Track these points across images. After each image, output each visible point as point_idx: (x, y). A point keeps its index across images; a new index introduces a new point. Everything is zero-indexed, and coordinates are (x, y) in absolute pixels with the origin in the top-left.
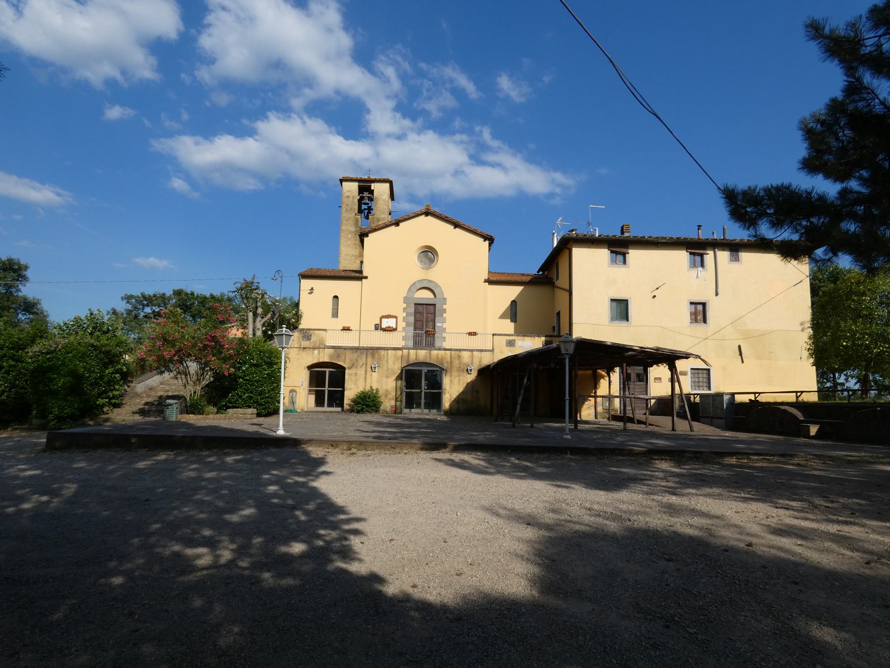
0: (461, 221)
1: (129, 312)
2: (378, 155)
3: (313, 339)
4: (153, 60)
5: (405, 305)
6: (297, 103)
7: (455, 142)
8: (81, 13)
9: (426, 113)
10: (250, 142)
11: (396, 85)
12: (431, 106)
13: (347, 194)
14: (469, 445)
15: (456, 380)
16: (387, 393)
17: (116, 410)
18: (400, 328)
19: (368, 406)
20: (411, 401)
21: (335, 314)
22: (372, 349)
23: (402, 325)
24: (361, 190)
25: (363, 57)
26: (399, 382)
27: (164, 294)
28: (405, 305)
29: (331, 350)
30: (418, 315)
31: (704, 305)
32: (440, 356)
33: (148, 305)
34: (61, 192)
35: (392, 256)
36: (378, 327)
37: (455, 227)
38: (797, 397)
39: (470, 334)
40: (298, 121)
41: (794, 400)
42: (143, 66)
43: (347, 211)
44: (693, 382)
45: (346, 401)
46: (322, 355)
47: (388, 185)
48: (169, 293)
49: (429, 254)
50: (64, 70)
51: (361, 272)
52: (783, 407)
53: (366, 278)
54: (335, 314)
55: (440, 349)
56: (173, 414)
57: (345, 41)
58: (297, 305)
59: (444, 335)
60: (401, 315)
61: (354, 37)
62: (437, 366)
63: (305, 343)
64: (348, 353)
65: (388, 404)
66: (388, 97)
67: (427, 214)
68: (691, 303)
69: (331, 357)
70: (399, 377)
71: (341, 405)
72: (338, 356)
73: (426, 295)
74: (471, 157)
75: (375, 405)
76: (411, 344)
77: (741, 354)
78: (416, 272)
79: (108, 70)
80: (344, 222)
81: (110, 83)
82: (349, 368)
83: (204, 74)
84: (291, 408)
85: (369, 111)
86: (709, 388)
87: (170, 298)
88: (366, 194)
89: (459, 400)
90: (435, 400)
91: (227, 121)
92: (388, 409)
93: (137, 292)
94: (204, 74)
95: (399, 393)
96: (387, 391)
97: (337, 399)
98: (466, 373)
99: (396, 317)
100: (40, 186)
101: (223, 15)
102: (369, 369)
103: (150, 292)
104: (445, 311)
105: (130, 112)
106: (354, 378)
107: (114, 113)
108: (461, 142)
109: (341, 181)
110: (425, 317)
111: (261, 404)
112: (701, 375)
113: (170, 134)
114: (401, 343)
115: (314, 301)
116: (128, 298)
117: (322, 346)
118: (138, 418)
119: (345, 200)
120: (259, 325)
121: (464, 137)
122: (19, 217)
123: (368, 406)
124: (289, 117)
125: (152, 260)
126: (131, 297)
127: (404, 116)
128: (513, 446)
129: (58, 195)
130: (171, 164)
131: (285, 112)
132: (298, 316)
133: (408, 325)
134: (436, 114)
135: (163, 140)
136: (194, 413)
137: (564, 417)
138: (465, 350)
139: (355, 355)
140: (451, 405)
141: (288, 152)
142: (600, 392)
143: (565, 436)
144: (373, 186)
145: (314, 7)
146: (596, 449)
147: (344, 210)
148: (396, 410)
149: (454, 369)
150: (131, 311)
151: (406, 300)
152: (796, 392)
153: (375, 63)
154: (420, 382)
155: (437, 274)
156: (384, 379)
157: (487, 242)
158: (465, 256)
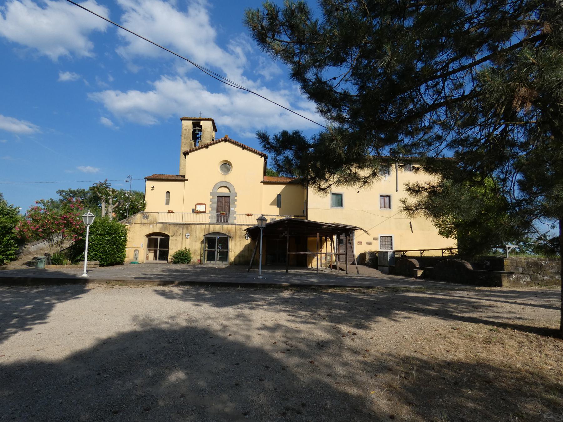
0: (247, 145)
1: (62, 201)
2: (232, 103)
3: (150, 218)
4: (91, 45)
5: (211, 197)
6: (181, 70)
7: (280, 95)
8: (44, 14)
9: (262, 77)
10: (151, 94)
11: (243, 60)
12: (266, 73)
13: (185, 128)
14: (187, 282)
15: (238, 243)
16: (195, 252)
17: (13, 263)
18: (207, 212)
19: (182, 259)
20: (211, 257)
21: (168, 203)
22: (186, 224)
23: (209, 209)
24: (194, 125)
25: (222, 42)
26: (203, 245)
27: (84, 190)
28: (211, 197)
29: (161, 225)
30: (219, 203)
31: (389, 197)
32: (229, 229)
33: (73, 197)
34: (32, 125)
35: (203, 167)
36: (195, 211)
37: (243, 149)
38: (421, 253)
39: (248, 215)
40: (182, 81)
41: (420, 255)
42: (82, 46)
43: (185, 138)
44: (382, 244)
45: (170, 257)
46: (155, 228)
47: (211, 122)
48: (87, 189)
49: (226, 166)
50: (35, 50)
51: (184, 176)
52: (409, 260)
53: (187, 180)
54: (168, 203)
55: (232, 224)
56: (42, 265)
57: (211, 32)
58: (144, 197)
59: (235, 215)
60: (209, 203)
61: (217, 30)
62: (225, 234)
63: (145, 221)
64: (171, 227)
65: (195, 258)
66: (238, 67)
67: (226, 140)
68: (381, 196)
69: (161, 229)
70: (202, 242)
71: (167, 259)
72: (165, 229)
73: (224, 191)
74: (292, 105)
75: (186, 259)
76: (214, 221)
77: (411, 227)
78: (218, 176)
79: (61, 51)
80: (183, 145)
81: (62, 58)
82: (172, 236)
83: (121, 51)
84: (135, 261)
85: (225, 75)
86: (392, 248)
87: (88, 192)
88: (197, 128)
89: (240, 256)
90: (224, 256)
91: (137, 82)
92: (196, 261)
93: (66, 189)
94: (121, 51)
95: (202, 251)
96: (195, 250)
97: (164, 255)
98: (244, 239)
99: (205, 205)
100: (18, 121)
101: (134, 14)
102: (184, 237)
103: (75, 188)
104: (236, 201)
105: (76, 76)
106: (175, 242)
107: (65, 77)
108: (285, 95)
109: (182, 120)
110: (223, 205)
111: (102, 259)
112: (386, 240)
113: (100, 90)
114: (208, 221)
115: (155, 195)
116: (61, 192)
117: (156, 223)
118: (25, 267)
119: (184, 132)
120: (110, 209)
121: (287, 92)
122: (4, 141)
123: (182, 259)
124: (176, 79)
125: (89, 168)
126: (62, 191)
127: (249, 78)
128: (213, 283)
129: (30, 127)
130: (101, 108)
131: (173, 75)
132: (144, 205)
133: (213, 209)
134: (268, 78)
135: (94, 93)
136: (54, 264)
137: (258, 265)
138: (244, 225)
139: (176, 228)
140: (235, 259)
141: (176, 101)
142: (324, 251)
143: (259, 277)
144: (202, 123)
145: (191, 11)
146: (260, 284)
147: (183, 138)
148: (200, 262)
149: (237, 236)
150: (63, 201)
151: (212, 194)
152: (421, 250)
153: (227, 45)
154: (215, 243)
155: (231, 178)
156: (194, 243)
157: (263, 158)
158: (250, 166)
